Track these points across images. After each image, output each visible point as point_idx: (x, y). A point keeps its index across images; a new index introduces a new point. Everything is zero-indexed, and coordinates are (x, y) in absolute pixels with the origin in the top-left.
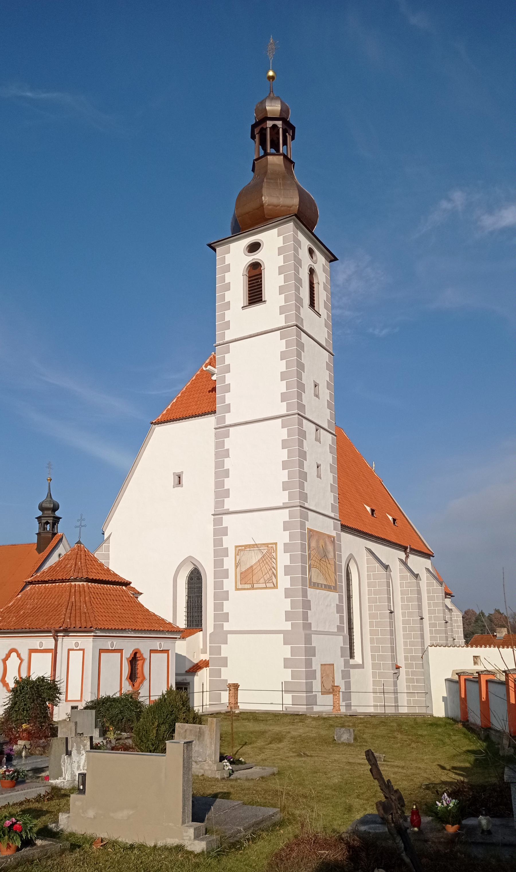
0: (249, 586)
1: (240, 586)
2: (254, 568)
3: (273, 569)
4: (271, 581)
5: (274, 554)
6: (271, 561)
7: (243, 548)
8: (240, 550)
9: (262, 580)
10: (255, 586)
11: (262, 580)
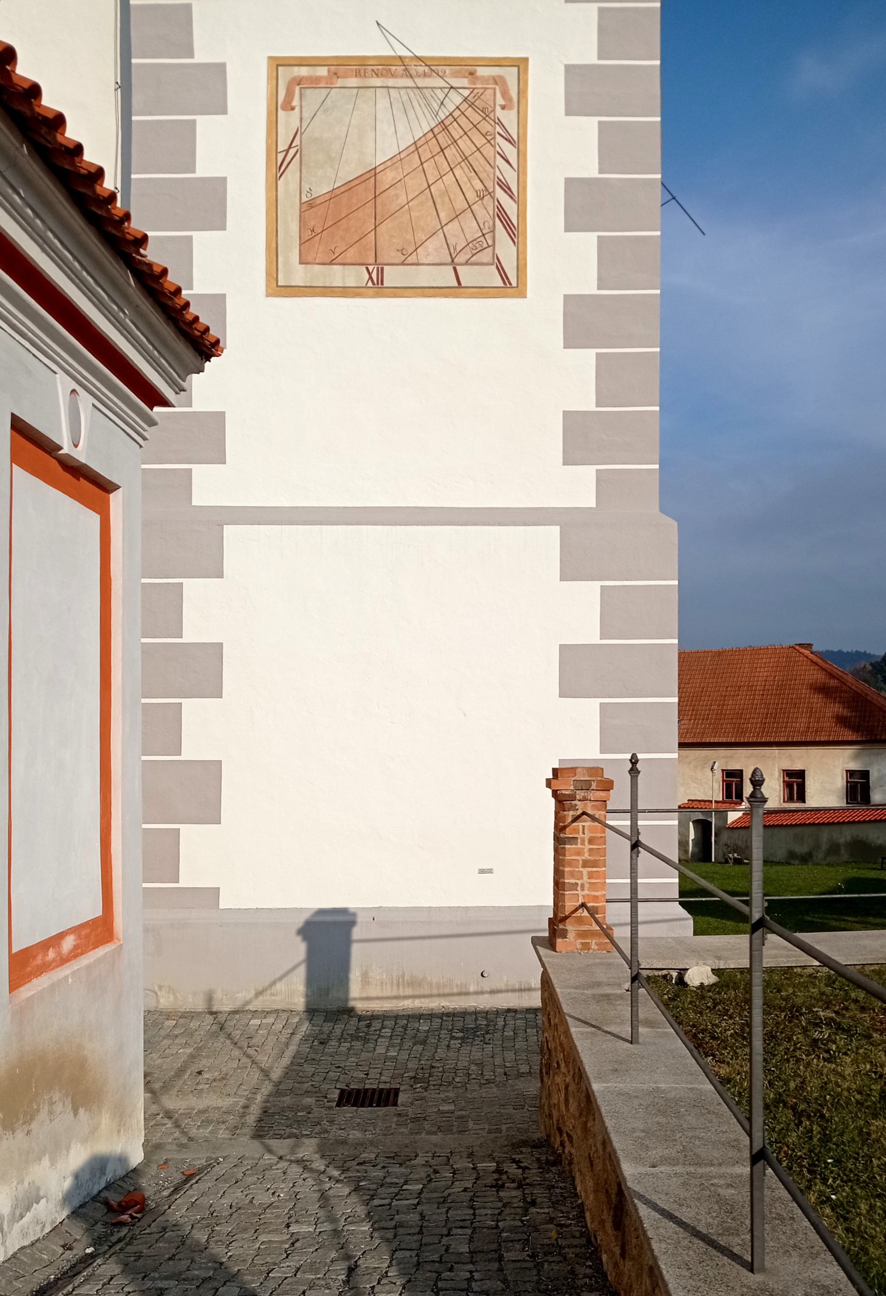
0: (356, 276)
1: (299, 275)
2: (388, 178)
3: (500, 194)
4: (486, 256)
5: (509, 118)
6: (488, 150)
7: (323, 71)
8: (299, 81)
9: (434, 249)
10: (393, 276)
11: (434, 249)
